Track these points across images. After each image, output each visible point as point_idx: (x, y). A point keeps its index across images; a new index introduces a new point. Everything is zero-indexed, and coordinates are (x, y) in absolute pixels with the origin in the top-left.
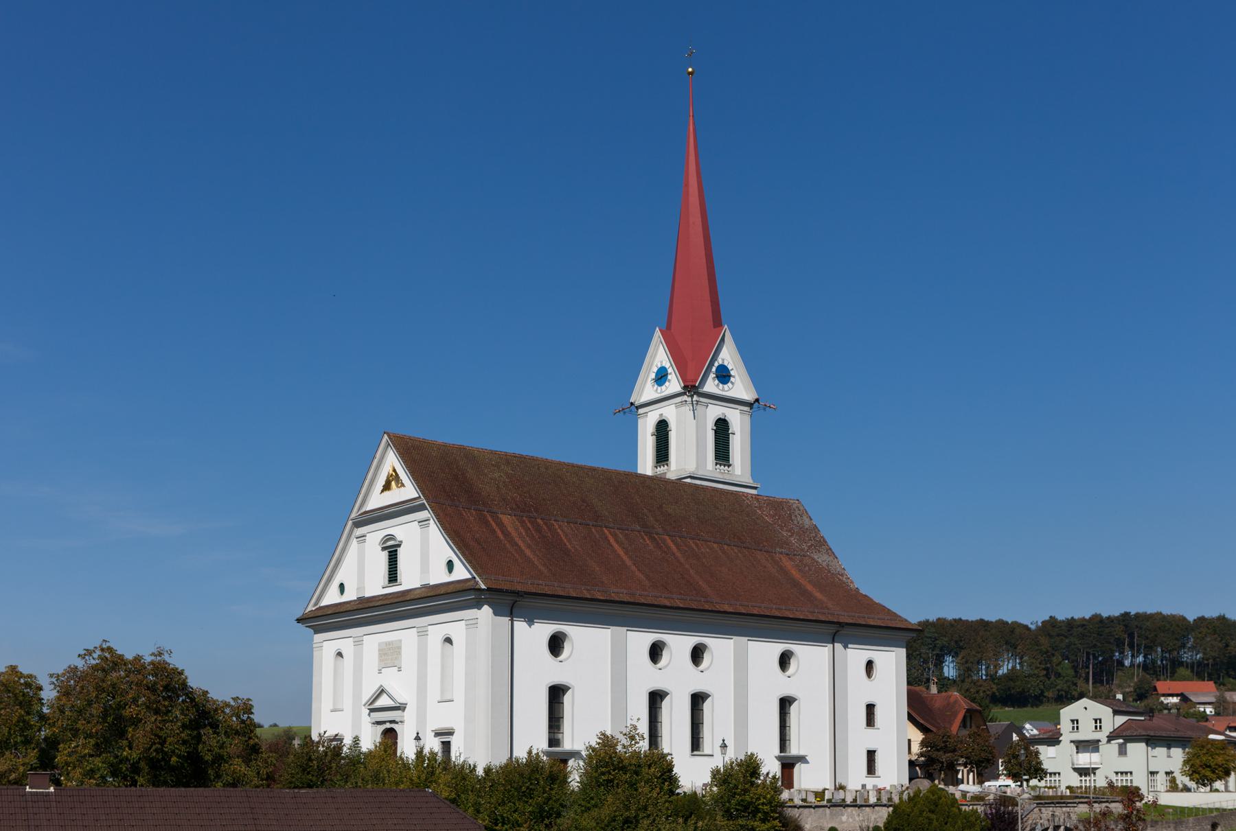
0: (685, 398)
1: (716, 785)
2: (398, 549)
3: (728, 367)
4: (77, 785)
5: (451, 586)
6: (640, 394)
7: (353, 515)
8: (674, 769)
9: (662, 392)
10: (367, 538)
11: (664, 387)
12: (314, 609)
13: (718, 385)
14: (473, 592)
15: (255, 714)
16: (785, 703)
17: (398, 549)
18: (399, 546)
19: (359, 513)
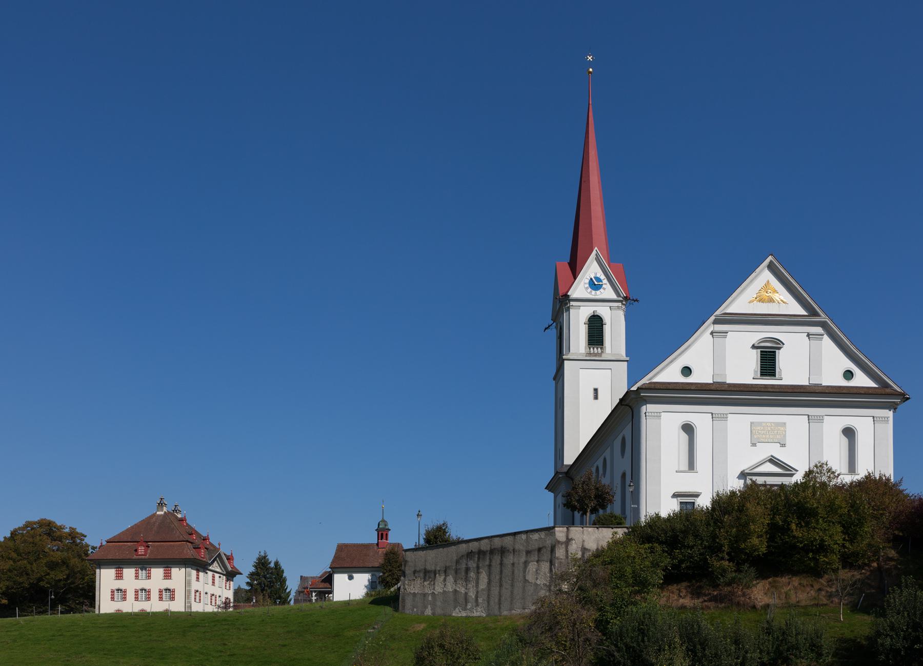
0: (620, 304)
2: (777, 351)
7: (718, 312)
11: (598, 292)
12: (648, 382)
17: (777, 351)
18: (779, 348)
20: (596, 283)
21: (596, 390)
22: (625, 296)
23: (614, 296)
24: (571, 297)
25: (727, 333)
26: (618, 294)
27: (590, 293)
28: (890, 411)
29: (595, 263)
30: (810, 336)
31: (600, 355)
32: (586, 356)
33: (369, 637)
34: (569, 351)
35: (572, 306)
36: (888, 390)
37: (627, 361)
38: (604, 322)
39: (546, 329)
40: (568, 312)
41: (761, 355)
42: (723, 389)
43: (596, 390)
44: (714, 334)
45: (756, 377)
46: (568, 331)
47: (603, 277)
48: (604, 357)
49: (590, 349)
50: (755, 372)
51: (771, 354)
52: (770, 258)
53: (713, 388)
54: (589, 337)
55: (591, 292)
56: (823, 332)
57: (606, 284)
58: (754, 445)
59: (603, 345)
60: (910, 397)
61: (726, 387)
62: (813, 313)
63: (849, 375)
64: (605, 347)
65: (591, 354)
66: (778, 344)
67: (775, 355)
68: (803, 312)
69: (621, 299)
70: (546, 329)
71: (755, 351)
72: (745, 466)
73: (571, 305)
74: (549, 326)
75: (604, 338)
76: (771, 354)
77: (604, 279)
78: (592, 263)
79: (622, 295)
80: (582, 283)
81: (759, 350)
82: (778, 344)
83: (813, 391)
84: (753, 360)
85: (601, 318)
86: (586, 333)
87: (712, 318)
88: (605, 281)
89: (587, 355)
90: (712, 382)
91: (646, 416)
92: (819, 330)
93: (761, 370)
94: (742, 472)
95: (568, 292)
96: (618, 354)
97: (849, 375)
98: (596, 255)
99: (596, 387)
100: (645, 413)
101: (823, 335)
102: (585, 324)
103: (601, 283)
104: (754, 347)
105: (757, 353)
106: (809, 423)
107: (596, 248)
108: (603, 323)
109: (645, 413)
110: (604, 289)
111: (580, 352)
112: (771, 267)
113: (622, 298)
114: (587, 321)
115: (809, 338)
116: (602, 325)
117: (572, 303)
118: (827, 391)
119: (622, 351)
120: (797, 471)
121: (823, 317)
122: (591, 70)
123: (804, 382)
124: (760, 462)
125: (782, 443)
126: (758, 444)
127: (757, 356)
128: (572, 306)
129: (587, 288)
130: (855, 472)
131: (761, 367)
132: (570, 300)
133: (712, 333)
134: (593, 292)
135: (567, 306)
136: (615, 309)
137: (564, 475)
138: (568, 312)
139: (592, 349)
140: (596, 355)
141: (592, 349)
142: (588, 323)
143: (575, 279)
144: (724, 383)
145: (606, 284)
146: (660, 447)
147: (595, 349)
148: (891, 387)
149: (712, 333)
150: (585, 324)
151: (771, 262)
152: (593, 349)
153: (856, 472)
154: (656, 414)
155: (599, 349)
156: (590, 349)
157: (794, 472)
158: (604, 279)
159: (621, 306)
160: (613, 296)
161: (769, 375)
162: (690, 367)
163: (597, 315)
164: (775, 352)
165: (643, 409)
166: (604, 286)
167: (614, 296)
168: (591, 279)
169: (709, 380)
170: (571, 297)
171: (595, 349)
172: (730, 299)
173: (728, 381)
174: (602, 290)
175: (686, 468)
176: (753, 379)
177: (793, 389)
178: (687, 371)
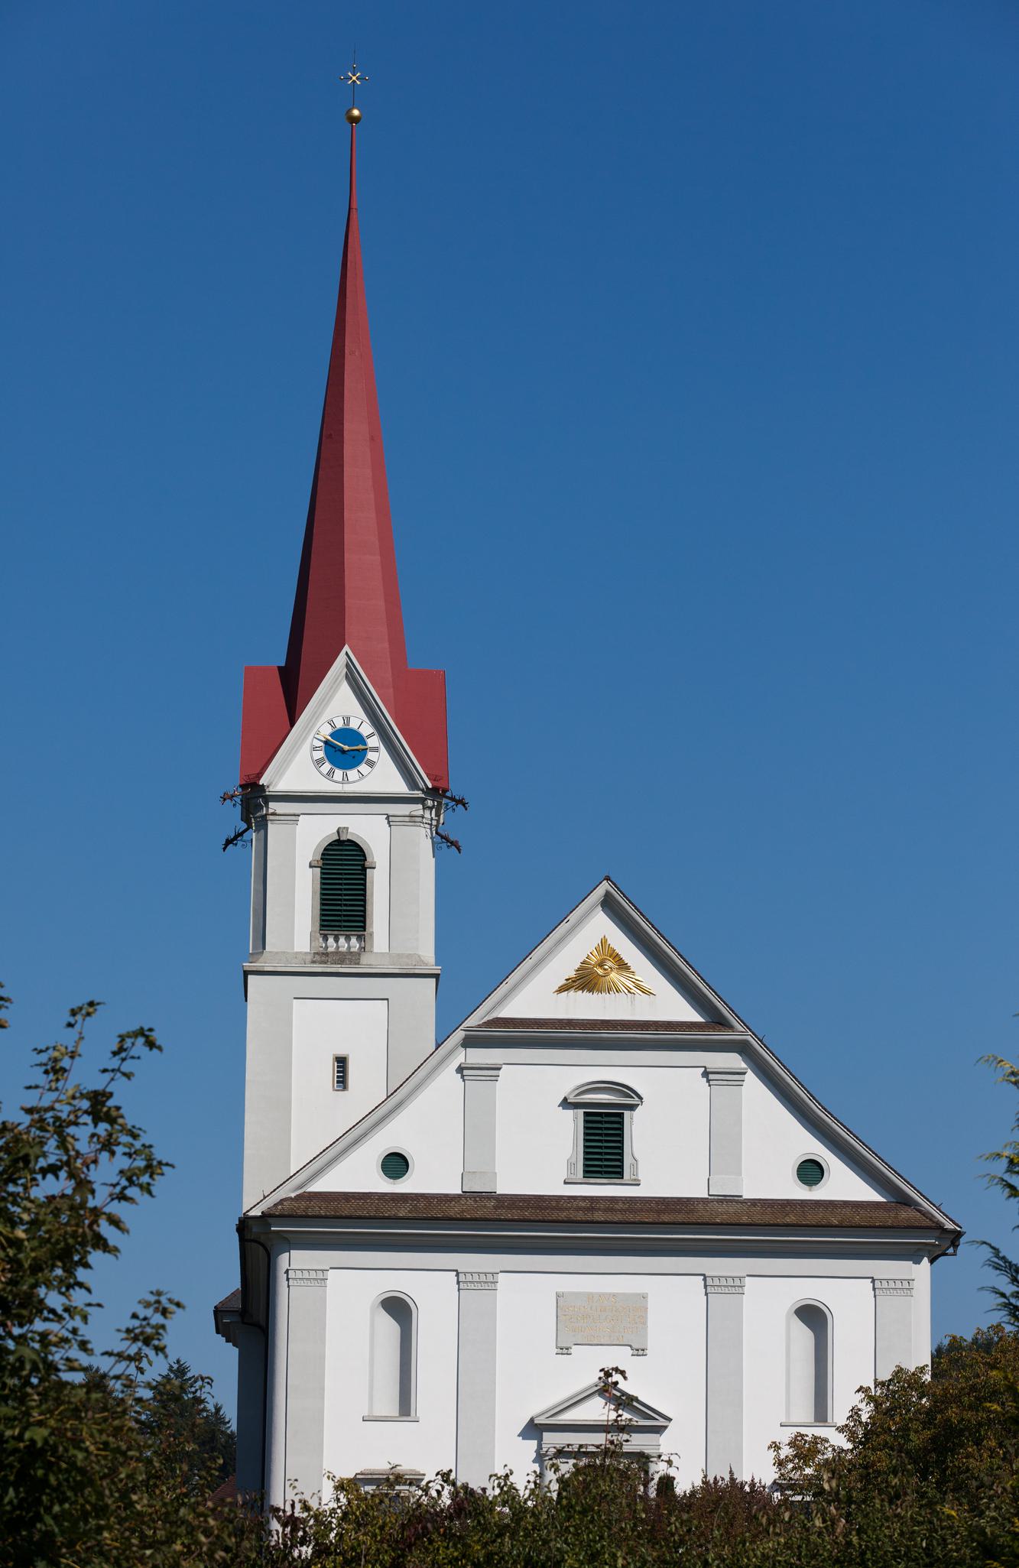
0: (417, 809)
1: (535, 1506)
2: (627, 1114)
3: (361, 730)
4: (194, 1425)
5: (732, 1208)
6: (280, 773)
7: (474, 1021)
8: (475, 1485)
9: (345, 780)
10: (501, 1073)
11: (352, 774)
12: (293, 1195)
13: (330, 774)
14: (937, 1233)
15: (91, 1340)
16: (213, 1397)
17: (627, 1114)
18: (632, 1107)
19: (485, 1020)
20: (346, 748)
21: (342, 1062)
22: (430, 786)
23: (400, 787)
24: (271, 789)
25: (499, 1069)
26: (412, 783)
27: (330, 775)
28: (918, 1262)
29: (345, 690)
30: (711, 1077)
31: (353, 958)
32: (313, 962)
33: (469, 1515)
34: (264, 948)
35: (274, 814)
36: (906, 1215)
37: (437, 976)
38: (369, 859)
39: (228, 842)
40: (262, 832)
41: (586, 1121)
42: (479, 1214)
43: (342, 1062)
44: (465, 1072)
45: (573, 1178)
46: (261, 888)
47: (367, 729)
48: (368, 963)
49: (325, 939)
50: (571, 1165)
51: (613, 1119)
52: (605, 886)
53: (454, 1210)
54: (322, 904)
55: (330, 774)
56: (744, 1065)
57: (376, 749)
58: (564, 1350)
59: (364, 928)
60: (963, 1230)
61: (488, 1210)
62: (717, 1021)
63: (811, 1171)
64: (371, 934)
65: (327, 954)
66: (630, 1097)
67: (622, 1123)
68: (693, 1016)
69: (419, 794)
70: (228, 842)
71: (570, 1113)
72: (536, 1406)
73: (270, 811)
74: (236, 837)
75: (368, 908)
76: (613, 1119)
77: (369, 736)
78: (334, 688)
79: (421, 785)
80: (306, 748)
81: (581, 1112)
82: (630, 1097)
83: (707, 1220)
84: (569, 1129)
85: (361, 850)
86: (314, 892)
87: (459, 1035)
88: (374, 741)
89: (317, 958)
90: (460, 1192)
91: (288, 1279)
92: (733, 1061)
93: (585, 1159)
94: (532, 1420)
95: (260, 775)
96: (409, 956)
97: (811, 1171)
98: (347, 666)
99: (341, 1053)
100: (287, 1272)
101: (744, 1073)
102: (311, 866)
103: (361, 747)
104: (566, 1104)
105: (576, 1118)
106: (706, 1294)
107: (346, 648)
108: (367, 864)
109: (287, 1272)
110: (371, 764)
111: (295, 950)
112: (609, 905)
113: (422, 790)
114: (319, 857)
115: (708, 1081)
116: (364, 869)
117: (273, 806)
118: (745, 1219)
119: (425, 951)
120: (670, 1420)
121: (739, 1033)
122: (356, 112)
123: (696, 1190)
124: (571, 1398)
125: (635, 1346)
126: (575, 1349)
127: (576, 1126)
128: (274, 814)
129: (319, 763)
130: (826, 1421)
131: (586, 1153)
132: (268, 799)
133: (460, 1070)
134: (338, 774)
135: (258, 814)
136: (403, 824)
137: (236, 1318)
138: (262, 832)
139: (331, 940)
140: (341, 957)
141: (331, 940)
142: (320, 864)
143: (292, 724)
144: (490, 1196)
145: (376, 749)
146: (322, 1357)
147: (342, 940)
148: (917, 1204)
149: (460, 1070)
150: (311, 866)
151: (608, 894)
152: (336, 940)
153: (829, 1420)
154: (313, 1275)
155: (354, 940)
156: (325, 939)
157: (661, 1422)
158: (369, 736)
159: (421, 812)
160: (398, 785)
161: (606, 1172)
162: (400, 1152)
163: (349, 840)
164: (621, 1115)
165: (283, 1261)
166: (371, 755)
167: (400, 787)
168: (327, 743)
169: (452, 1187)
170: (271, 789)
171: (342, 940)
172: (503, 988)
173: (504, 1188)
174: (363, 768)
175: (394, 1411)
176: (565, 1183)
177: (659, 1212)
178: (396, 1164)
